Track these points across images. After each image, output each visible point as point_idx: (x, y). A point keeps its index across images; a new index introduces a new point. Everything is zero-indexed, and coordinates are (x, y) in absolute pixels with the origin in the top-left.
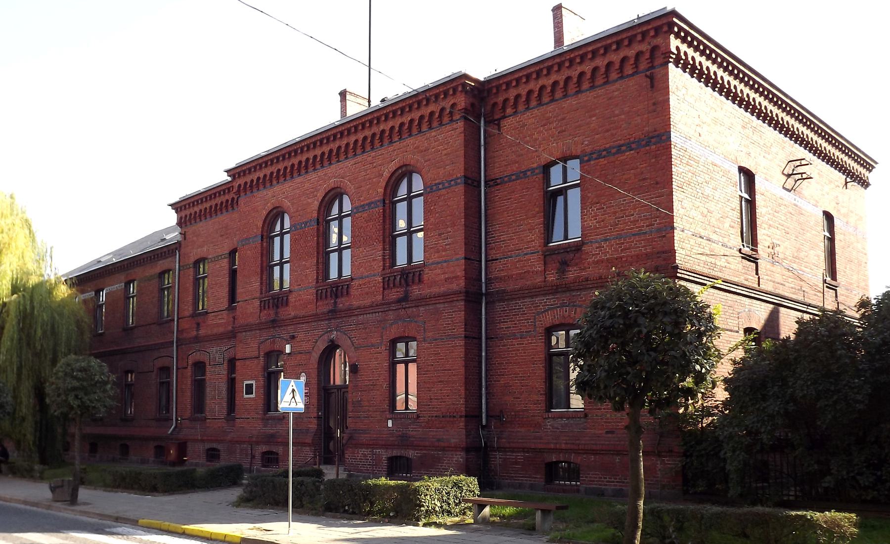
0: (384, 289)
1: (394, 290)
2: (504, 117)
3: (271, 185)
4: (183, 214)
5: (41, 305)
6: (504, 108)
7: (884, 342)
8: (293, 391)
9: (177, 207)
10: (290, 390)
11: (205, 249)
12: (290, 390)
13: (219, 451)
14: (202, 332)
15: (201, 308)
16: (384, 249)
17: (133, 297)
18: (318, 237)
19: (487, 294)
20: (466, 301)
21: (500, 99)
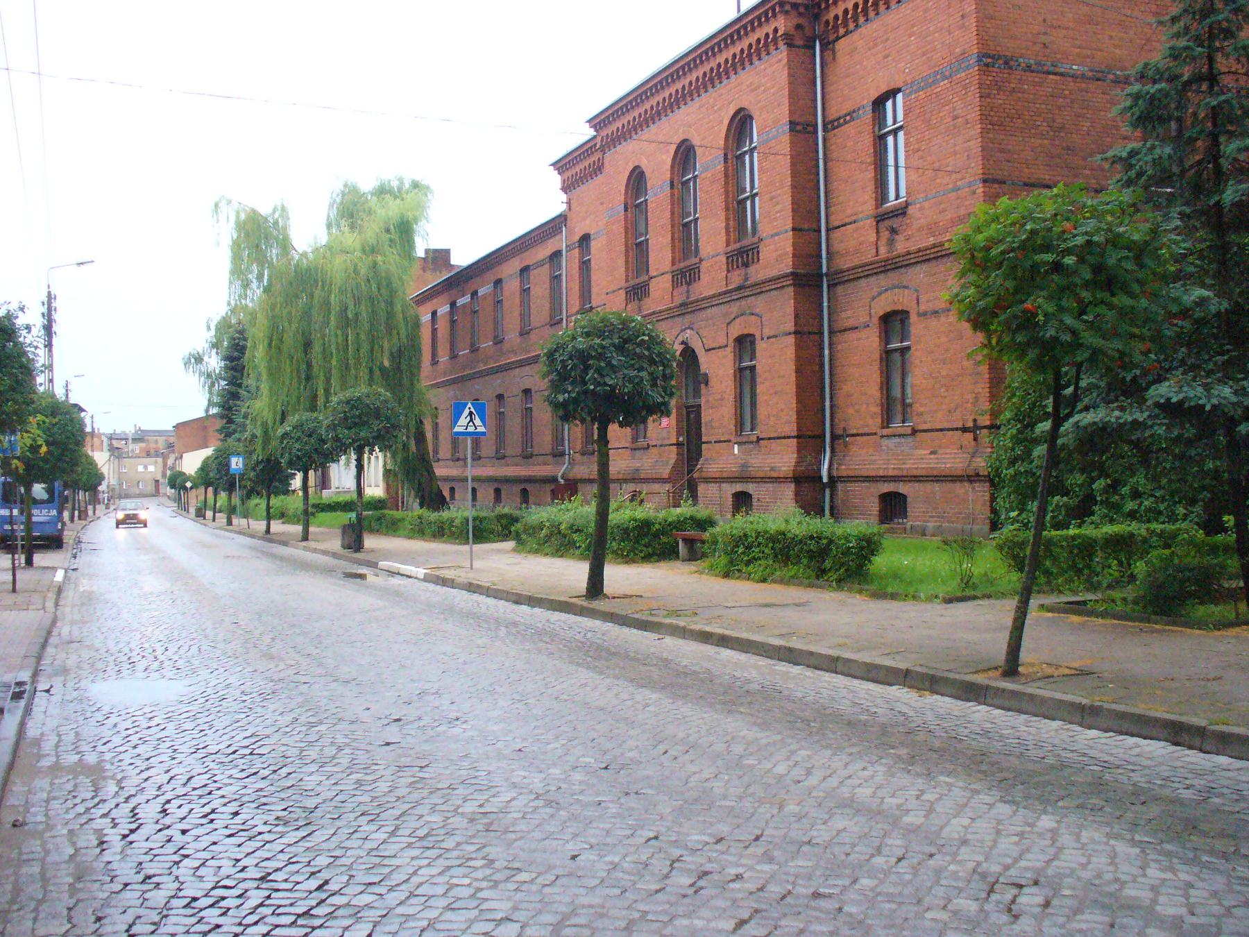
0: (728, 271)
1: (738, 272)
2: (838, 38)
3: (768, 54)
4: (569, 174)
5: (405, 319)
6: (836, 27)
7: (1237, 309)
8: (471, 413)
9: (561, 165)
10: (467, 412)
11: (588, 222)
12: (467, 412)
13: (905, 497)
14: (901, 246)
15: (892, 195)
16: (727, 219)
17: (895, 132)
18: (672, 204)
19: (827, 275)
20: (794, 285)
21: (831, 16)
